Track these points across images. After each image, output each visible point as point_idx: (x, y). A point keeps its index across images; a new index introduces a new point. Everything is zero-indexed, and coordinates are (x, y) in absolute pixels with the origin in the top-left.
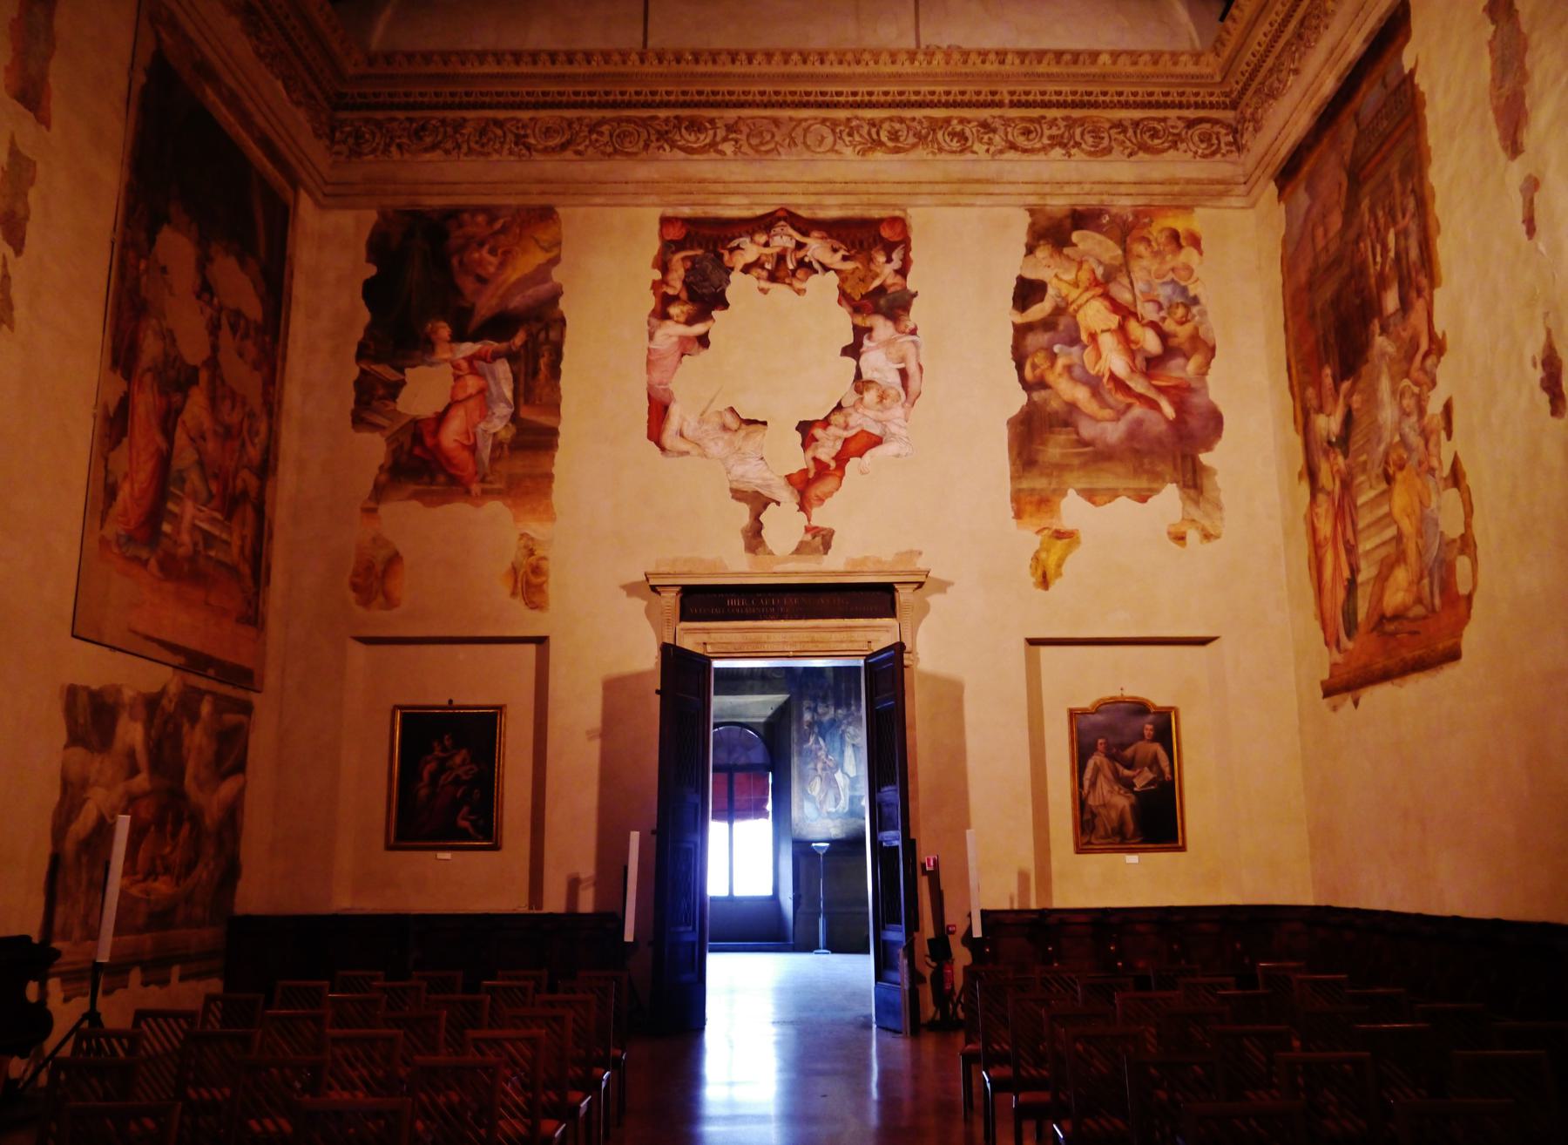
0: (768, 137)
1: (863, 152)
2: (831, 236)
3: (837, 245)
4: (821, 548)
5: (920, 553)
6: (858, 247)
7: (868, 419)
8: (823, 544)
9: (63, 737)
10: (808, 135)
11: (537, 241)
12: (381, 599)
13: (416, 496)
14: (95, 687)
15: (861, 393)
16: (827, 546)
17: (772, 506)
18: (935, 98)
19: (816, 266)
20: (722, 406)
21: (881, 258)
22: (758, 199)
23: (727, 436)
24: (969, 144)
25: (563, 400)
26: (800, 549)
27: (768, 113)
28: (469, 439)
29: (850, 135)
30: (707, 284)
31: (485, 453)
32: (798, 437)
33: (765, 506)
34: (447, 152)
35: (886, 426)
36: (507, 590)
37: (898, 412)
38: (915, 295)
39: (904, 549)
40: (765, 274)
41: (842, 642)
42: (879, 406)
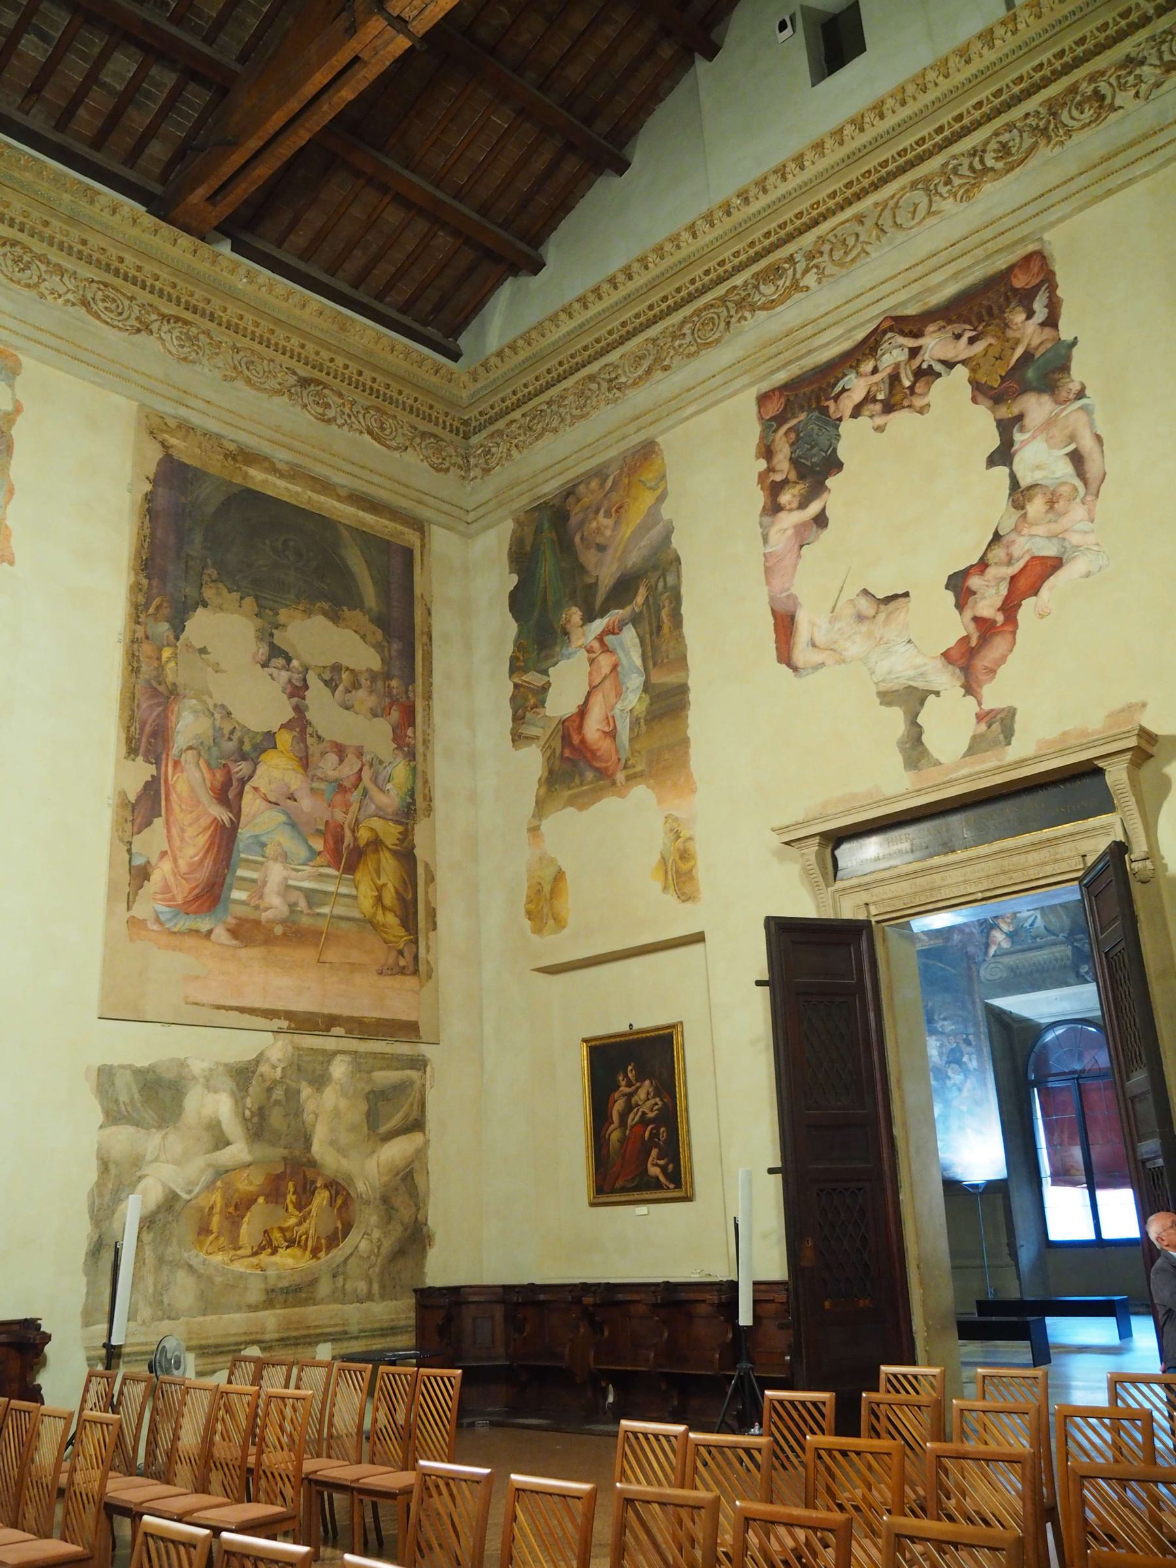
0: (851, 241)
1: (967, 196)
2: (950, 322)
3: (958, 328)
4: (1001, 737)
5: (1144, 705)
6: (986, 318)
7: (1038, 539)
8: (1003, 732)
9: (99, 1117)
10: (898, 212)
11: (643, 483)
12: (551, 922)
13: (571, 802)
14: (142, 1063)
15: (1023, 508)
16: (1008, 734)
17: (932, 697)
18: (1046, 72)
19: (938, 367)
20: (852, 591)
21: (1019, 317)
22: (852, 322)
23: (864, 628)
24: (1108, 101)
25: (689, 647)
26: (976, 746)
27: (849, 213)
28: (608, 723)
29: (948, 182)
30: (815, 450)
31: (624, 734)
32: (950, 597)
33: (922, 702)
34: (555, 430)
35: (1064, 539)
36: (659, 886)
37: (1078, 512)
38: (1075, 342)
39: (1117, 706)
40: (878, 407)
41: (1044, 864)
42: (1050, 516)
